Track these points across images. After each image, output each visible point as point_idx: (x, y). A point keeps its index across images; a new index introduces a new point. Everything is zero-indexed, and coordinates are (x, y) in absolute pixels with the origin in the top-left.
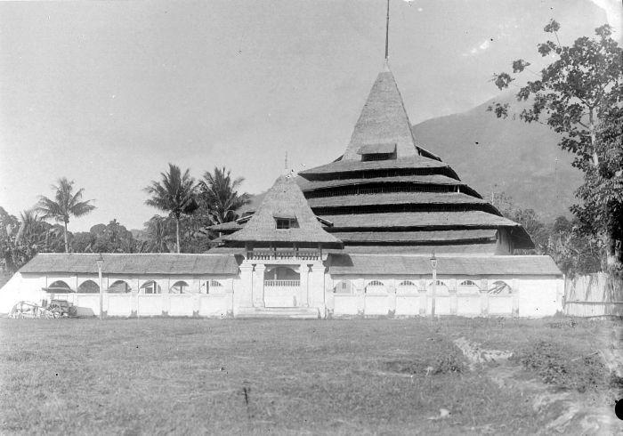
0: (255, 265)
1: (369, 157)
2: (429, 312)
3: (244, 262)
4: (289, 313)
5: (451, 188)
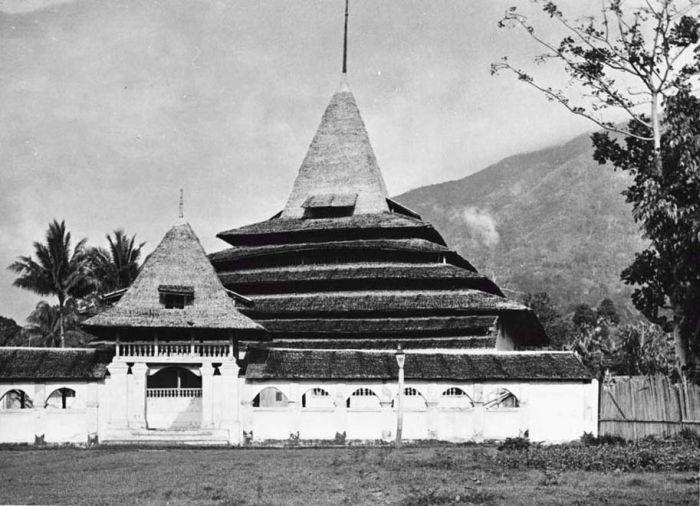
0: (131, 365)
1: (313, 212)
2: (394, 437)
3: (115, 359)
4: (183, 438)
5: (435, 257)
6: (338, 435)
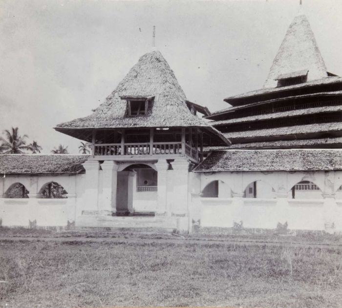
1: (283, 82)
6: (279, 225)
